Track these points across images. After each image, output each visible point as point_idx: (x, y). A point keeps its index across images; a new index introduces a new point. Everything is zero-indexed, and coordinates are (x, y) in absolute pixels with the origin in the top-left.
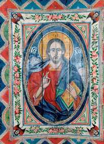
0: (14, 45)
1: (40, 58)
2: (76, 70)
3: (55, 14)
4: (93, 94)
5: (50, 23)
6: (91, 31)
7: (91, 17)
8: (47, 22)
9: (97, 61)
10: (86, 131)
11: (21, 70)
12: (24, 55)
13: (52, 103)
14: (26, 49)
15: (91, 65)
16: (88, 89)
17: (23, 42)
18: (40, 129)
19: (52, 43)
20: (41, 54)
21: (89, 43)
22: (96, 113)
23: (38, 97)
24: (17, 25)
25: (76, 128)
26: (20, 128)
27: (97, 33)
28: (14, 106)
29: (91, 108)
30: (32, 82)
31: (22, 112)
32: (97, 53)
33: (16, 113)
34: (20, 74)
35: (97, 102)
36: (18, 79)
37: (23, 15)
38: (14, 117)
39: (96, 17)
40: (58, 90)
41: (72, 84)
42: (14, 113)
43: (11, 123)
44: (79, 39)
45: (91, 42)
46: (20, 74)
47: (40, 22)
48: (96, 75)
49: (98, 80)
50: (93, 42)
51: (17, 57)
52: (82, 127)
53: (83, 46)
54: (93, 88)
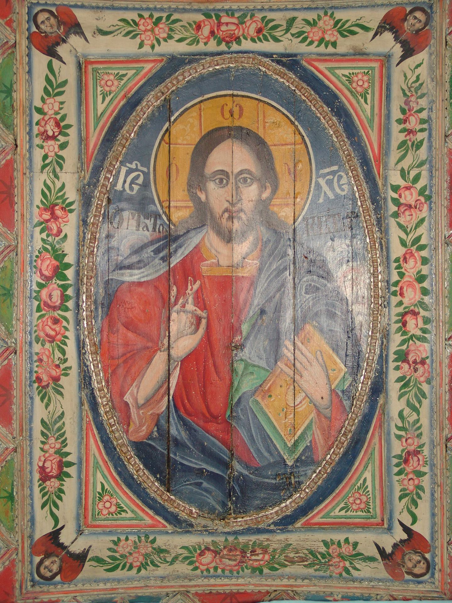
0: (38, 154)
1: (157, 216)
2: (327, 275)
3: (230, 13)
4: (405, 382)
5: (206, 54)
6: (396, 92)
7: (393, 29)
8: (194, 48)
9: (422, 230)
10: (372, 559)
11: (70, 273)
12: (87, 201)
13: (213, 427)
14: (97, 171)
15: (397, 251)
16: (383, 359)
17: (83, 140)
18: (160, 551)
19: (218, 143)
20: (164, 197)
21: (384, 149)
22: (420, 474)
23: (149, 401)
24: (56, 63)
25: (325, 543)
26: (62, 547)
27: (423, 102)
28: (37, 445)
29: (397, 448)
30: (122, 329)
31: (72, 470)
32: (421, 192)
33: (45, 477)
34: (64, 288)
35: (425, 421)
36: (58, 313)
37: (81, 16)
38: (37, 490)
39: (418, 31)
40: (239, 367)
41: (306, 341)
42: (37, 476)
43: (22, 522)
44: (341, 128)
45: (394, 144)
46: (64, 288)
47: (157, 49)
48: (418, 296)
49: (427, 321)
50: (404, 143)
51: (51, 209)
52: (353, 538)
53: (356, 162)
54: (403, 357)
